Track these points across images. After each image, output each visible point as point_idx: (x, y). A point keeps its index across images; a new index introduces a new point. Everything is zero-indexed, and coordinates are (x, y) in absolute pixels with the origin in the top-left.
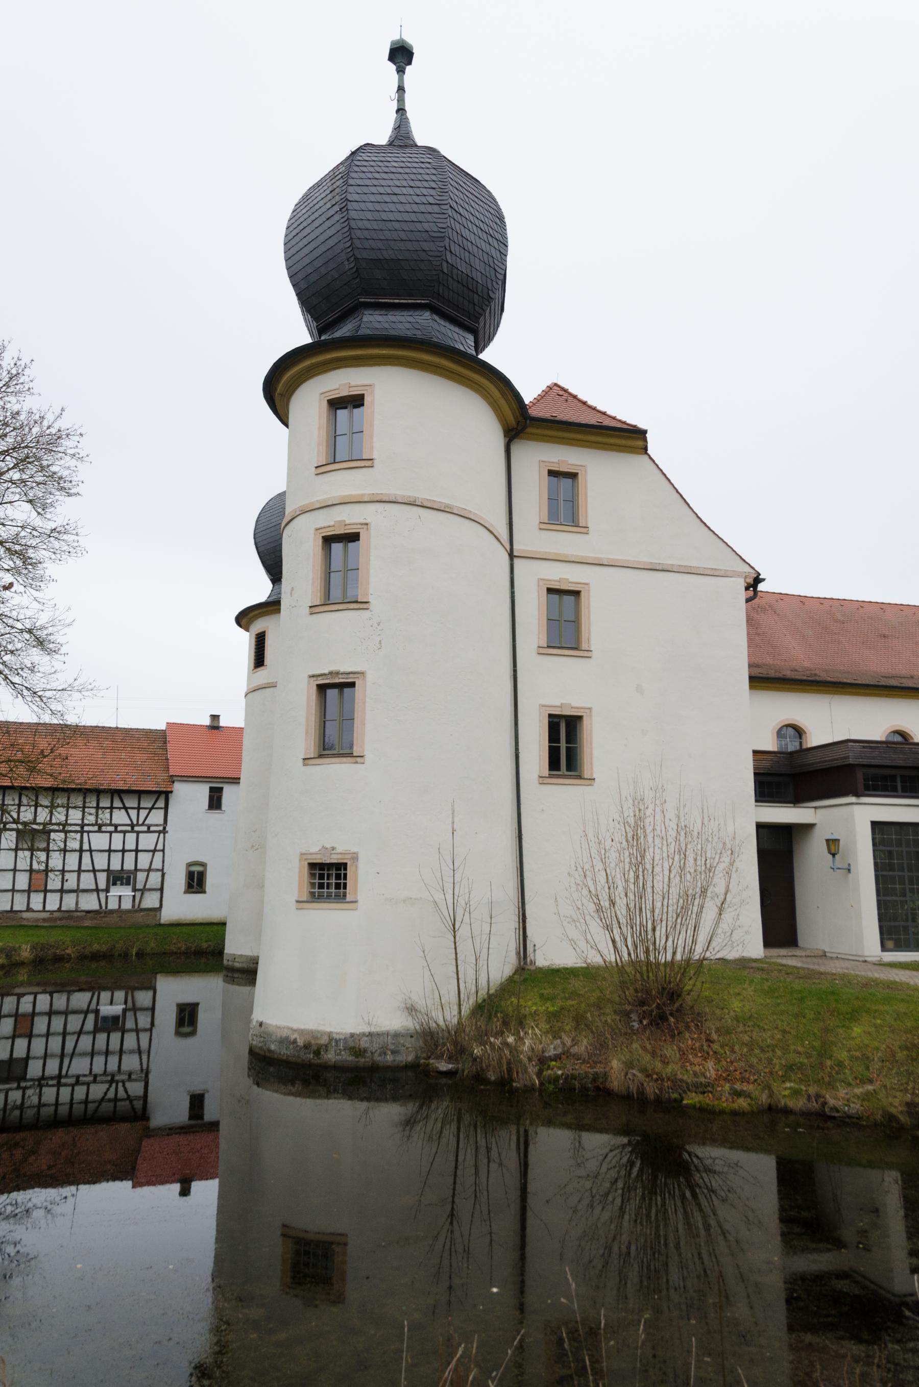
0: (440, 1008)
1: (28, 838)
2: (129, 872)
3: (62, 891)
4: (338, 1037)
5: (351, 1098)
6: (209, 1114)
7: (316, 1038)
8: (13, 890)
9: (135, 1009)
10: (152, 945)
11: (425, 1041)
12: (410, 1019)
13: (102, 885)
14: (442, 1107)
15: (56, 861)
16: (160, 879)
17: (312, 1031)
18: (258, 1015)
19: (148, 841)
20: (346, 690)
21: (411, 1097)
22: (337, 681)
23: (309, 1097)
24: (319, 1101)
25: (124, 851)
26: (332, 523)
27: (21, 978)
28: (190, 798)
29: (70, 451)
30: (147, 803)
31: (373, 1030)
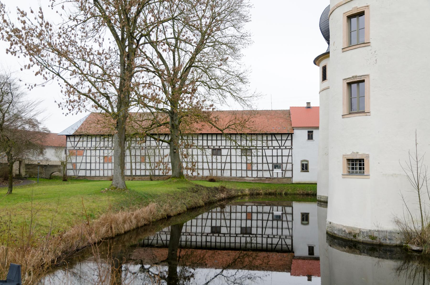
0: (412, 222)
1: (245, 151)
2: (280, 164)
3: (257, 170)
4: (363, 231)
5: (370, 256)
6: (316, 253)
7: (354, 230)
8: (242, 170)
9: (286, 214)
10: (290, 191)
11: (405, 236)
12: (397, 226)
13: (271, 169)
14: (415, 265)
15: (254, 160)
16: (291, 167)
17: (352, 228)
18: (329, 219)
19: (286, 152)
20: (360, 84)
21: (399, 259)
22: (356, 80)
23: (352, 253)
24: (357, 255)
25: (277, 156)
26: (351, 9)
27: (246, 200)
28: (300, 135)
29: (247, 5)
30: (284, 138)
31: (379, 229)
